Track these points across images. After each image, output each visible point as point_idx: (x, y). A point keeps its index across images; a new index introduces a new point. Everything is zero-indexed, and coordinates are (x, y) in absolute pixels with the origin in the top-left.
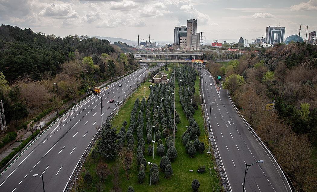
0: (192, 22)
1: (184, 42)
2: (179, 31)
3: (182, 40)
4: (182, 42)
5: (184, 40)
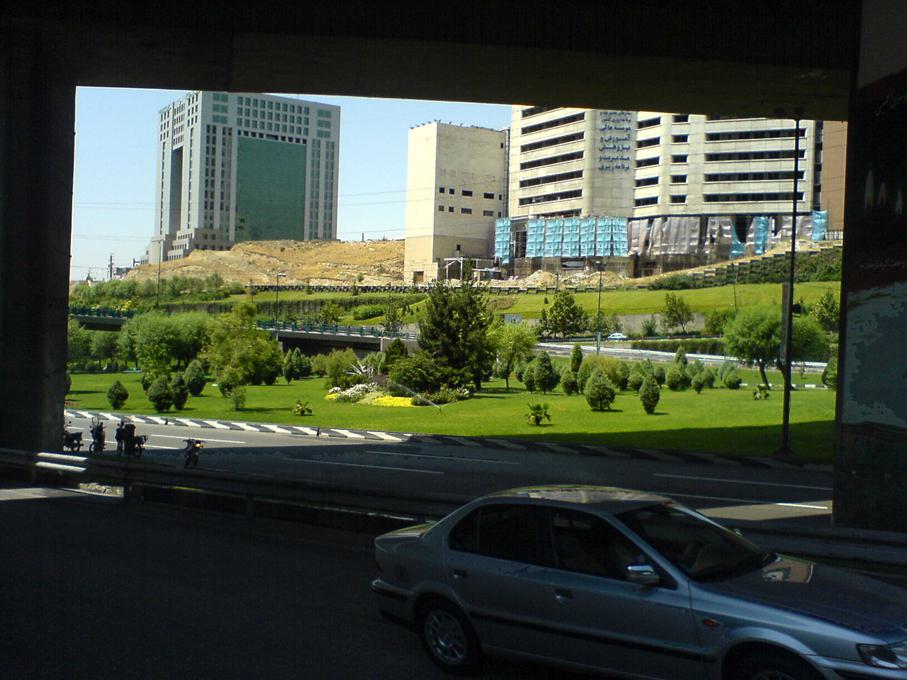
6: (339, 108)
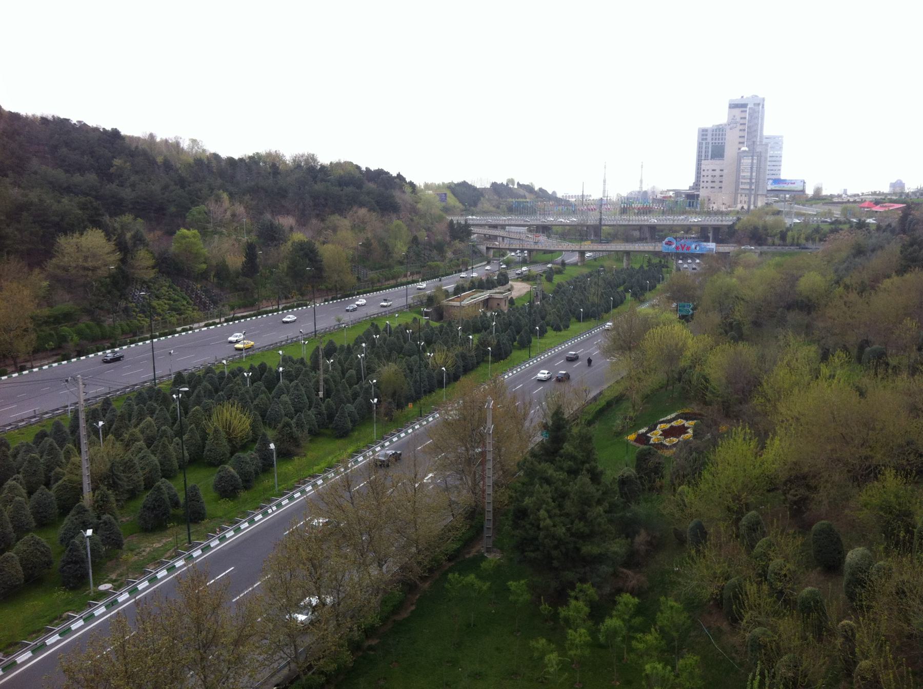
0: (744, 106)
1: (717, 179)
2: (709, 140)
3: (710, 173)
4: (710, 179)
5: (718, 173)
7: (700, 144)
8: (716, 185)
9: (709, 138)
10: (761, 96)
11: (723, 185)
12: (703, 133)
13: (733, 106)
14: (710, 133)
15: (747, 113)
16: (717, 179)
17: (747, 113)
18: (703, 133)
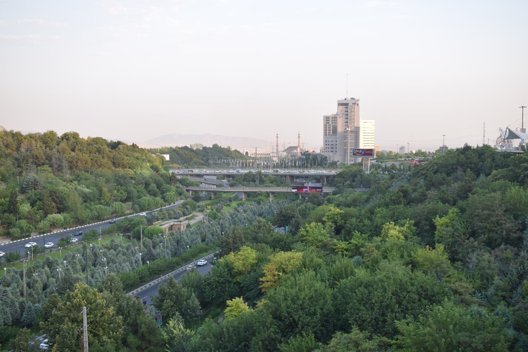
2: (331, 123)
3: (330, 143)
6: (324, 116)
7: (325, 126)
8: (334, 150)
9: (330, 122)
10: (356, 98)
11: (337, 150)
12: (327, 119)
13: (340, 104)
14: (331, 119)
15: (347, 107)
16: (334, 146)
17: (347, 107)
18: (327, 119)
